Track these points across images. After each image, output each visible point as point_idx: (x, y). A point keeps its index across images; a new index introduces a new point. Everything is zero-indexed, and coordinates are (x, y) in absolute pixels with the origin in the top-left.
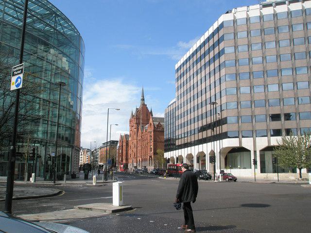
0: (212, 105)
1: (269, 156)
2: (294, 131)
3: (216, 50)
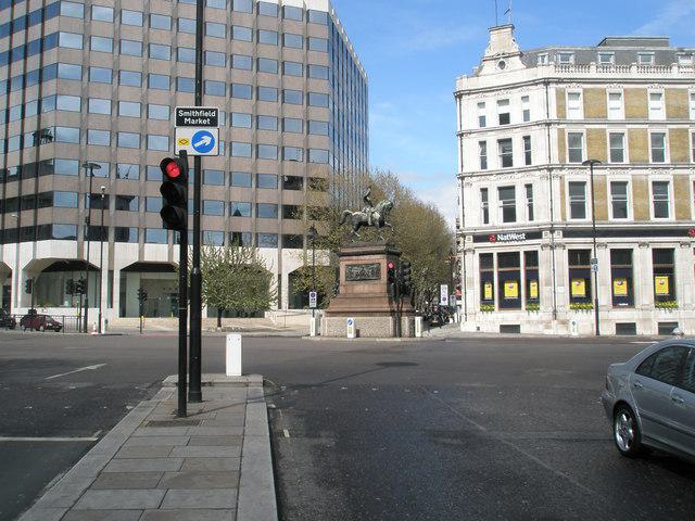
0: (89, 170)
1: (135, 282)
2: (133, 233)
3: (35, 32)
